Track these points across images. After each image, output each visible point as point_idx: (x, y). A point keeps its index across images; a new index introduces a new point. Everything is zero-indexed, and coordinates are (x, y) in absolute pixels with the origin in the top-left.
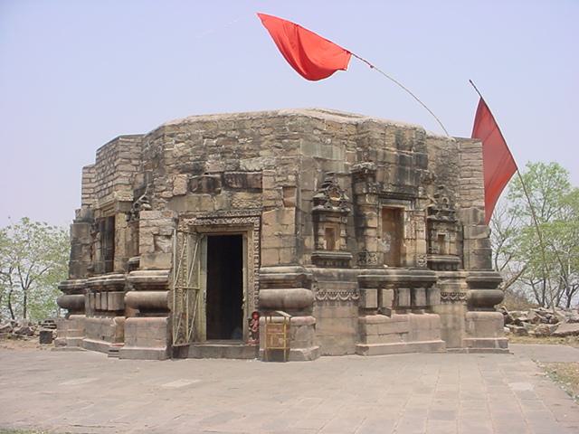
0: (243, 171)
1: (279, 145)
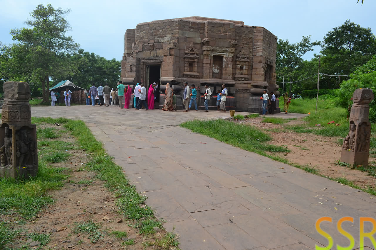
0: (160, 42)
1: (172, 32)
